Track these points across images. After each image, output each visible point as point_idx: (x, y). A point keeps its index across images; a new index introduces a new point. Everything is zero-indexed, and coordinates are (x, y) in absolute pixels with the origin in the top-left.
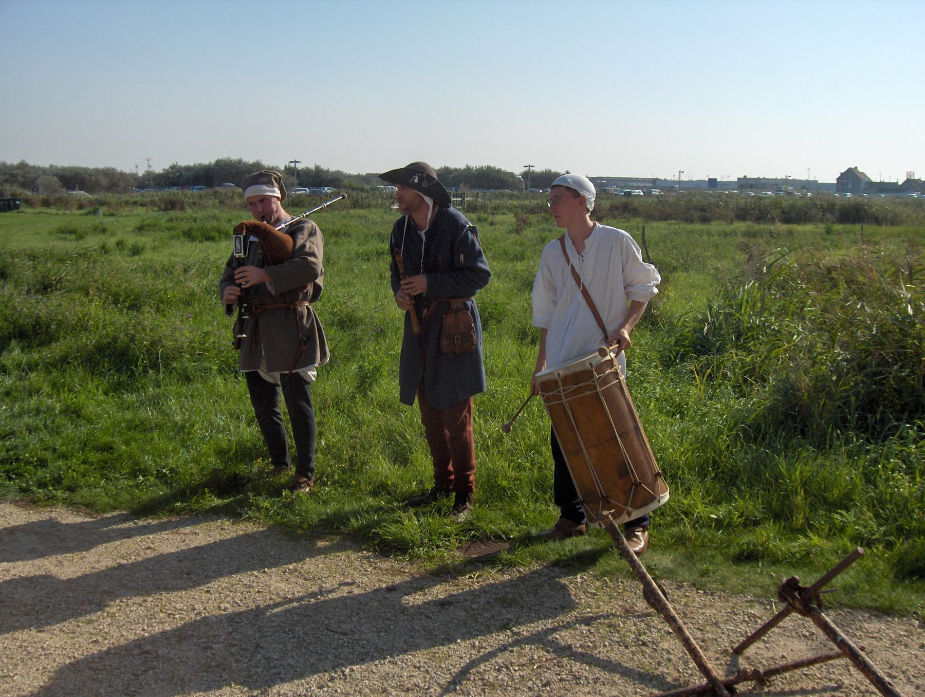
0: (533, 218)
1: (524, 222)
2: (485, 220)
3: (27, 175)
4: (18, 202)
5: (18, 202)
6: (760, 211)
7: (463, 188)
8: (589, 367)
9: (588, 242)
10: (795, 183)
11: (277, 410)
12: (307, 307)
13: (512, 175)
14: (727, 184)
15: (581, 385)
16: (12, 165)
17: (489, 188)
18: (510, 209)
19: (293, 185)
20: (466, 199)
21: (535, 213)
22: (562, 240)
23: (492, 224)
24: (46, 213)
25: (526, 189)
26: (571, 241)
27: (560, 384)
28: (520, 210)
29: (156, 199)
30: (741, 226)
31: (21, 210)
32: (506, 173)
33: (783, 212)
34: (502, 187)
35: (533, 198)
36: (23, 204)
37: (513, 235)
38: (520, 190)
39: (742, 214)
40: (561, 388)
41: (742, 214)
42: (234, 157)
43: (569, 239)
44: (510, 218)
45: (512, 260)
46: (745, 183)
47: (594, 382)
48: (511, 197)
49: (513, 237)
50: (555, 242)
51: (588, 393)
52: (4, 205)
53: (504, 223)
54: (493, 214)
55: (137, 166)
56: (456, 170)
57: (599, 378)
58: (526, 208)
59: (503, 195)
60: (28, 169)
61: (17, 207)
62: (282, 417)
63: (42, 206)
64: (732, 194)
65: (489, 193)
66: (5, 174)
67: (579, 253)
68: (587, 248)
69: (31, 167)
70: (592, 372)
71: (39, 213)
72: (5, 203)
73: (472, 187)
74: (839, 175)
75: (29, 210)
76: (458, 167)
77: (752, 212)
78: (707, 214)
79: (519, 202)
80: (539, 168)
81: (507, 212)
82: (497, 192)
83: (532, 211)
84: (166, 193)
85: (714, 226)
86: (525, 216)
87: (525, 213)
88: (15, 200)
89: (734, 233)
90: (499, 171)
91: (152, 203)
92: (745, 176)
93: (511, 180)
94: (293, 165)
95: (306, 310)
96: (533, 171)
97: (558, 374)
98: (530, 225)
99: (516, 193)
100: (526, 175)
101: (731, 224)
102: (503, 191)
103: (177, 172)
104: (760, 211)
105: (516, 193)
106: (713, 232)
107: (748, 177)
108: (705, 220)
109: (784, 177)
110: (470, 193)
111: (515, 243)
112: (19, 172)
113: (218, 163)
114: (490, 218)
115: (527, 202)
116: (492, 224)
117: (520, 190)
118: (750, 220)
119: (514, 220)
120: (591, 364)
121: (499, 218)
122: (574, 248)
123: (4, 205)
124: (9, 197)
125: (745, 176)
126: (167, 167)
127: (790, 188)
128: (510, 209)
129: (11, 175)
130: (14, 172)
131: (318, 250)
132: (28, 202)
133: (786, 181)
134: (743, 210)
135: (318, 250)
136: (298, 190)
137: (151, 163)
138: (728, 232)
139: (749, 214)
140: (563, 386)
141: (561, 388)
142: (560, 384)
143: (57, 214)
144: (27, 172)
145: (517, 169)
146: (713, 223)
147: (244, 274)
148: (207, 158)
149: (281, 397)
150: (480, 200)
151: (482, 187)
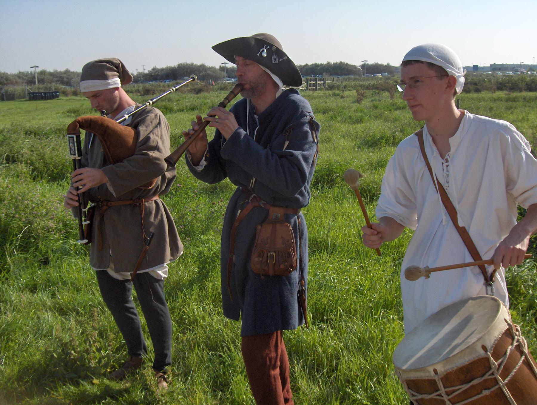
0: (368, 93)
1: (362, 95)
2: (338, 95)
3: (69, 77)
4: (58, 94)
5: (58, 94)
6: (512, 84)
7: (325, 76)
8: (482, 352)
9: (453, 141)
10: (525, 66)
11: (128, 305)
12: (156, 202)
13: (355, 67)
14: (483, 68)
15: (475, 382)
16: (61, 72)
17: (341, 75)
18: (354, 87)
19: (224, 77)
20: (327, 82)
21: (369, 89)
22: (420, 135)
23: (342, 97)
24: (74, 99)
25: (363, 75)
26: (431, 139)
27: (440, 385)
28: (359, 88)
29: (140, 88)
30: (501, 94)
31: (59, 98)
32: (351, 66)
33: (527, 84)
34: (349, 74)
35: (368, 80)
36: (61, 94)
37: (356, 104)
38: (360, 75)
39: (501, 86)
40: (443, 391)
41: (501, 86)
42: (189, 62)
43: (429, 136)
44: (354, 93)
45: (354, 123)
46: (495, 68)
47: (493, 374)
48: (354, 80)
49: (355, 106)
50: (412, 137)
51: (486, 393)
52: (50, 95)
53: (350, 96)
54: (343, 91)
55: (137, 70)
56: (321, 65)
57: (500, 365)
58: (364, 86)
59: (349, 79)
60: (70, 74)
61: (57, 96)
62: (136, 311)
63: (73, 95)
64: (489, 74)
65: (341, 78)
66: (57, 77)
67: (442, 156)
68: (453, 150)
69: (72, 72)
70: (488, 359)
71: (70, 99)
72: (51, 94)
73: (331, 75)
74: (493, 64)
75: (64, 98)
76: (323, 63)
77: (507, 85)
78: (479, 87)
79: (359, 82)
80: (371, 62)
81: (351, 88)
82: (346, 77)
83: (368, 88)
84: (148, 85)
85: (484, 94)
86: (363, 91)
87: (363, 89)
88: (56, 92)
89: (499, 99)
90: (347, 64)
91: (138, 91)
92: (495, 63)
93: (354, 70)
94: (224, 65)
95: (154, 205)
96: (368, 64)
97: (435, 371)
98: (366, 97)
99: (357, 77)
100: (363, 66)
101: (494, 92)
102: (350, 76)
103: (156, 72)
104: (512, 84)
105: (357, 77)
106: (487, 99)
107: (496, 64)
108: (477, 91)
109: (519, 64)
110: (329, 78)
111: (356, 111)
112: (65, 75)
113: (179, 65)
114: (341, 93)
115: (364, 83)
116: (342, 97)
117: (360, 75)
118: (506, 90)
119: (356, 94)
120: (484, 348)
121: (346, 93)
122: (434, 148)
123: (50, 95)
124: (54, 91)
125: (495, 63)
126: (150, 69)
127: (523, 70)
128: (354, 87)
129: (61, 77)
130: (62, 75)
131: (163, 143)
132: (65, 93)
133: (521, 66)
134: (501, 84)
135: (163, 143)
136: (227, 80)
137: (145, 68)
138: (496, 99)
139: (505, 86)
140: (445, 388)
141: (443, 391)
142: (440, 385)
143: (80, 100)
144: (69, 76)
145: (358, 63)
146: (483, 92)
147: (80, 177)
148: (173, 63)
149: (133, 293)
150: (335, 82)
151: (336, 74)
